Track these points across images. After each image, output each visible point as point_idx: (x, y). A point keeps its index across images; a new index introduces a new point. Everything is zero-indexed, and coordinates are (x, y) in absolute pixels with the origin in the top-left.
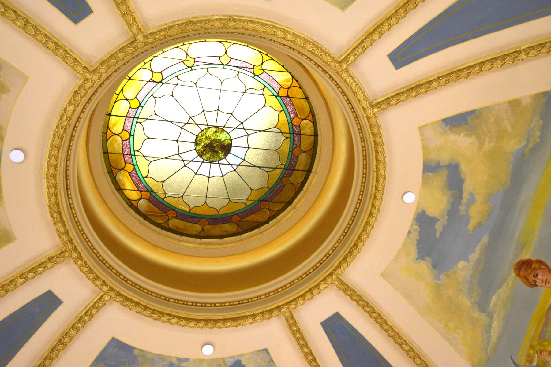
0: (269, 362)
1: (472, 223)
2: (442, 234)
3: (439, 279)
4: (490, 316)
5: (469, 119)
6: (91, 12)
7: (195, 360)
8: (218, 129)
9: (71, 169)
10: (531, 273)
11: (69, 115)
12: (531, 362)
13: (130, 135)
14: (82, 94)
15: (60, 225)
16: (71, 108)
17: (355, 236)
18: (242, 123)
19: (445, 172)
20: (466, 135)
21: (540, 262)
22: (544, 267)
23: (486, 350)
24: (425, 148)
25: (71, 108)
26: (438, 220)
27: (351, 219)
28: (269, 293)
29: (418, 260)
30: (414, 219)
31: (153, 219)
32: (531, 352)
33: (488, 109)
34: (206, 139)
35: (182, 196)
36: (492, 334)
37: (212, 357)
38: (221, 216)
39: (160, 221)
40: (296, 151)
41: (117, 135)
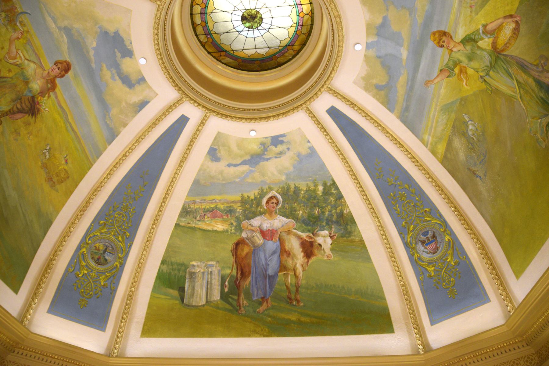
2: (114, 52)
3: (99, 27)
4: (59, 28)
6: (327, 111)
10: (62, 68)
12: (20, 22)
13: (299, 15)
19: (133, 82)
21: (63, 76)
22: (59, 76)
24: (150, 87)
26: (121, 58)
29: (116, 31)
30: (133, 51)
32: (26, 29)
33: (134, 117)
36: (50, 18)
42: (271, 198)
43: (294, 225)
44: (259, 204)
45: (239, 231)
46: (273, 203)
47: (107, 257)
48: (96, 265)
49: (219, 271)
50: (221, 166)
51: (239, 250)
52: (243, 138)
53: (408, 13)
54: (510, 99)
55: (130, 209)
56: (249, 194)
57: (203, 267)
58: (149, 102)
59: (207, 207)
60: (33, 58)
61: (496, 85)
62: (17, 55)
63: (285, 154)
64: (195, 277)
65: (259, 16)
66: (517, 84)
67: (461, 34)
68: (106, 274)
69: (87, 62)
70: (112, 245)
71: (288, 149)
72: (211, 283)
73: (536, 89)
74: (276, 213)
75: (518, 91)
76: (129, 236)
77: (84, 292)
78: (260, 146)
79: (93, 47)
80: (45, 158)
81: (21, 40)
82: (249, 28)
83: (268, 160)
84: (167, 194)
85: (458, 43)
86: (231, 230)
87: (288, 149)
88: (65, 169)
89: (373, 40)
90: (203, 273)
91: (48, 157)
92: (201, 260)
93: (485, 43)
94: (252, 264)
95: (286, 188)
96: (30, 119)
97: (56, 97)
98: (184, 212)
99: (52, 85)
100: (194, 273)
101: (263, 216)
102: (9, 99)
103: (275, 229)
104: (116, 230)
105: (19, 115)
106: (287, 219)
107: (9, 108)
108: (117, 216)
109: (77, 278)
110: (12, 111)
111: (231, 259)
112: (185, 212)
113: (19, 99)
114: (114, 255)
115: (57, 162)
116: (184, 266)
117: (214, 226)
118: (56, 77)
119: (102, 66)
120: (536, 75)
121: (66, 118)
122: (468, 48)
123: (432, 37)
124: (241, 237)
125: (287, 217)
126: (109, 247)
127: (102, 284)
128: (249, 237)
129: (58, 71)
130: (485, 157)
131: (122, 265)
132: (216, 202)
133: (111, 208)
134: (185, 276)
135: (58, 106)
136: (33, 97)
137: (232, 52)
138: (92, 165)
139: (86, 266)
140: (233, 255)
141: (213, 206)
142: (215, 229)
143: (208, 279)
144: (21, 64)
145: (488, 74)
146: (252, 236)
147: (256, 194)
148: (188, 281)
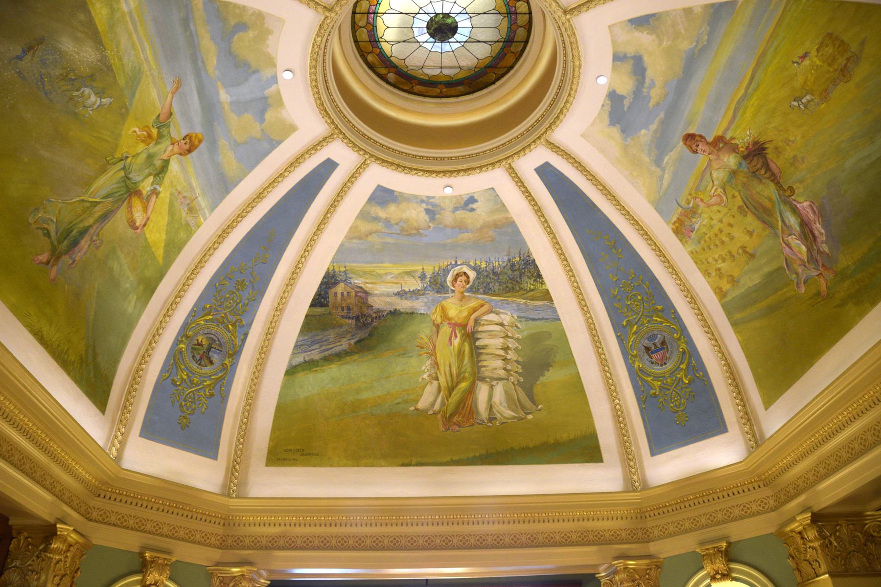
0: (495, 196)
2: (629, 108)
3: (626, 141)
4: (663, 170)
5: (651, 21)
7: (439, 198)
8: (447, 15)
9: (328, 48)
10: (694, 143)
11: (318, 44)
12: (689, 204)
14: (325, 28)
15: (326, 118)
16: (319, 39)
17: (558, 109)
18: (465, 9)
19: (631, 62)
21: (701, 136)
23: (659, 192)
24: (614, 42)
25: (319, 39)
28: (492, 149)
30: (607, 96)
31: (401, 86)
33: (667, 13)
34: (436, 23)
35: (422, 68)
36: (664, 182)
39: (406, 88)
40: (514, 27)
41: (363, 27)
53: (239, 141)
54: (87, 183)
60: (708, 176)
61: (111, 170)
62: (716, 195)
66: (95, 202)
67: (174, 167)
69: (666, 124)
73: (81, 225)
75: (90, 200)
79: (647, 132)
80: (812, 100)
81: (701, 197)
85: (170, 156)
88: (818, 50)
89: (270, 89)
91: (808, 97)
93: (146, 187)
96: (770, 148)
97: (727, 129)
99: (718, 143)
105: (772, 166)
110: (772, 178)
115: (812, 74)
118: (708, 143)
120: (91, 231)
121: (743, 101)
122: (158, 163)
123: (200, 136)
129: (701, 144)
130: (46, 94)
135: (736, 121)
136: (745, 158)
144: (721, 188)
145: (124, 168)
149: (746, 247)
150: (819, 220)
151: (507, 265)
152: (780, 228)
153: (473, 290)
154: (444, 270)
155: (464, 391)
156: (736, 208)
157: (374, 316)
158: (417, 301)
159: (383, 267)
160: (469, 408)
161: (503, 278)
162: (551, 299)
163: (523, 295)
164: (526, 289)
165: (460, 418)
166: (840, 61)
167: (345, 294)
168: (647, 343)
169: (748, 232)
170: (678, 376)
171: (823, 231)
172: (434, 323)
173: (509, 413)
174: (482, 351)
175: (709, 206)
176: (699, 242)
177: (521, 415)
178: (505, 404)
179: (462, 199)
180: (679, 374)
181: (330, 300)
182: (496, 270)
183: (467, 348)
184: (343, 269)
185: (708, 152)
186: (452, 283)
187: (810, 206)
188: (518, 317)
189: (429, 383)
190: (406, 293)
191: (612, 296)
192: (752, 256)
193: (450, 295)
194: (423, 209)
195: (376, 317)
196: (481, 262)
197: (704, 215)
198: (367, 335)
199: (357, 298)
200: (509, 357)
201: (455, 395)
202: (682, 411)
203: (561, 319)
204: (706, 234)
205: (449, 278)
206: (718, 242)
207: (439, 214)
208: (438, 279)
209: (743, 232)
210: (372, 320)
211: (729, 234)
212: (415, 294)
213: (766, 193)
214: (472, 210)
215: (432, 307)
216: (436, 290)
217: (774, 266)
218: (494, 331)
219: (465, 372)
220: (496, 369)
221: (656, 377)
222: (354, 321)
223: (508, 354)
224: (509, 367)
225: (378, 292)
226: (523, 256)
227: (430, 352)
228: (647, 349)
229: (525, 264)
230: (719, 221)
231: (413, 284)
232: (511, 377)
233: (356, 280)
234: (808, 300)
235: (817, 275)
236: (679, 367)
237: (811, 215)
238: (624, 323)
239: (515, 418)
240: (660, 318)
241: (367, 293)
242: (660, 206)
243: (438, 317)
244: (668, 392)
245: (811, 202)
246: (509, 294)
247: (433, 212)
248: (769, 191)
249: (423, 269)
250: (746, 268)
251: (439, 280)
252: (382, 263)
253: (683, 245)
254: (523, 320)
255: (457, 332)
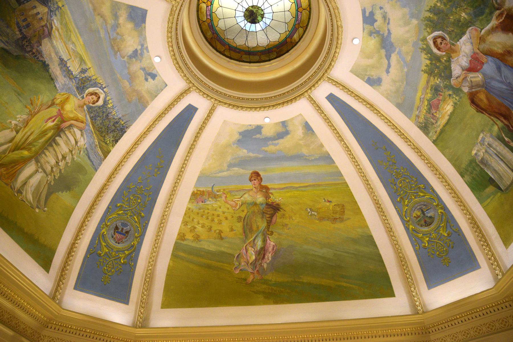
1: (266, 149)
2: (255, 138)
3: (233, 145)
4: (228, 170)
7: (149, 55)
10: (255, 178)
12: (217, 192)
19: (284, 130)
20: (303, 132)
21: (261, 179)
27: (181, 51)
30: (257, 125)
32: (222, 190)
33: (316, 137)
36: (220, 174)
37: (153, 62)
38: (214, 29)
40: (259, 54)
42: (435, 43)
43: (476, 30)
44: (438, 59)
45: (460, 92)
46: (441, 43)
47: (429, 215)
48: (428, 228)
49: (491, 136)
50: (387, 80)
51: (480, 104)
52: (361, 51)
55: (401, 172)
56: (424, 64)
57: (480, 147)
58: (307, 122)
59: (426, 108)
60: (241, 193)
63: (386, 13)
64: (486, 161)
65: (251, 8)
68: (441, 225)
69: (257, 160)
70: (422, 204)
71: (381, 8)
72: (499, 153)
74: (453, 44)
76: (424, 186)
77: (440, 253)
78: (372, 36)
80: (316, 216)
81: (228, 196)
82: (262, 18)
83: (389, 32)
84: (401, 134)
86: (456, 99)
87: (381, 8)
88: (335, 205)
90: (486, 151)
91: (316, 213)
92: (474, 145)
94: (500, 100)
95: (428, 23)
97: (275, 189)
98: (424, 130)
100: (482, 159)
101: (452, 60)
102: (260, 220)
103: (472, 54)
104: (412, 193)
105: (274, 219)
106: (466, 35)
107: (266, 222)
108: (401, 185)
109: (427, 248)
111: (482, 119)
112: (425, 128)
113: (263, 213)
114: (431, 208)
116: (473, 162)
117: (446, 112)
118: (260, 184)
119: (264, 150)
121: (294, 188)
124: (467, 94)
125: (464, 33)
126: (422, 207)
127: (446, 235)
128: (470, 86)
129: (257, 181)
131: (445, 208)
132: (423, 98)
133: (392, 186)
134: (482, 169)
135: (282, 190)
136: (267, 204)
137: (288, 33)
138: (346, 183)
139: (423, 235)
140: (482, 113)
141: (426, 103)
142: (450, 113)
143: (494, 152)
144: (242, 202)
146: (470, 82)
147: (426, 56)
148: (487, 170)
149: (222, 232)
150: (272, 253)
151: (116, 119)
152: (250, 241)
153: (90, 110)
154: (95, 83)
155: (22, 156)
156: (238, 215)
157: (34, 51)
158: (63, 77)
159: (77, 37)
160: (14, 171)
161: (107, 122)
162: (105, 157)
163: (101, 140)
164: (105, 140)
165: (5, 173)
166: (337, 215)
167: (40, 16)
168: (119, 224)
169: (232, 228)
170: (120, 255)
171: (270, 259)
172: (54, 99)
173: (30, 197)
174: (54, 145)
175: (226, 202)
176: (200, 209)
177: (34, 205)
178: (33, 189)
179: (152, 71)
180: (122, 255)
181: (26, 4)
182: (110, 115)
183: (50, 134)
184: (60, 4)
185: (255, 186)
186: (89, 93)
187: (274, 245)
188: (86, 148)
189: (10, 130)
190: (65, 65)
191: (128, 186)
192: (222, 238)
193: (79, 97)
194: (136, 48)
195: (34, 53)
196: (111, 103)
197: (218, 203)
198: (15, 54)
199: (41, 28)
200: (60, 164)
201: (16, 154)
202: (109, 275)
203: (97, 172)
204: (208, 210)
205: (91, 90)
206: (210, 218)
207: (136, 60)
208: (87, 82)
209: (229, 226)
210: (30, 51)
211: (221, 220)
212: (68, 73)
213: (260, 224)
214: (146, 80)
215: (65, 90)
216: (78, 86)
217: (230, 251)
218: (70, 141)
219: (34, 146)
220: (49, 163)
221: (108, 246)
222: (20, 36)
223: (62, 161)
224: (54, 169)
225: (55, 44)
226: (126, 125)
227: (33, 112)
228: (117, 228)
229: (121, 129)
230: (223, 212)
231: (74, 67)
232: (50, 176)
233: (57, 20)
234: (236, 278)
235: (251, 272)
236: (124, 251)
237: (270, 249)
238: (119, 205)
239: (30, 203)
240: (138, 219)
241: (50, 35)
242: (202, 178)
243: (60, 99)
244: (108, 259)
245: (276, 245)
246: (97, 132)
247: (137, 55)
248: (262, 225)
249: (90, 68)
250: (212, 240)
251: (86, 84)
252: (81, 35)
253: (189, 202)
254: (86, 152)
255: (57, 120)
